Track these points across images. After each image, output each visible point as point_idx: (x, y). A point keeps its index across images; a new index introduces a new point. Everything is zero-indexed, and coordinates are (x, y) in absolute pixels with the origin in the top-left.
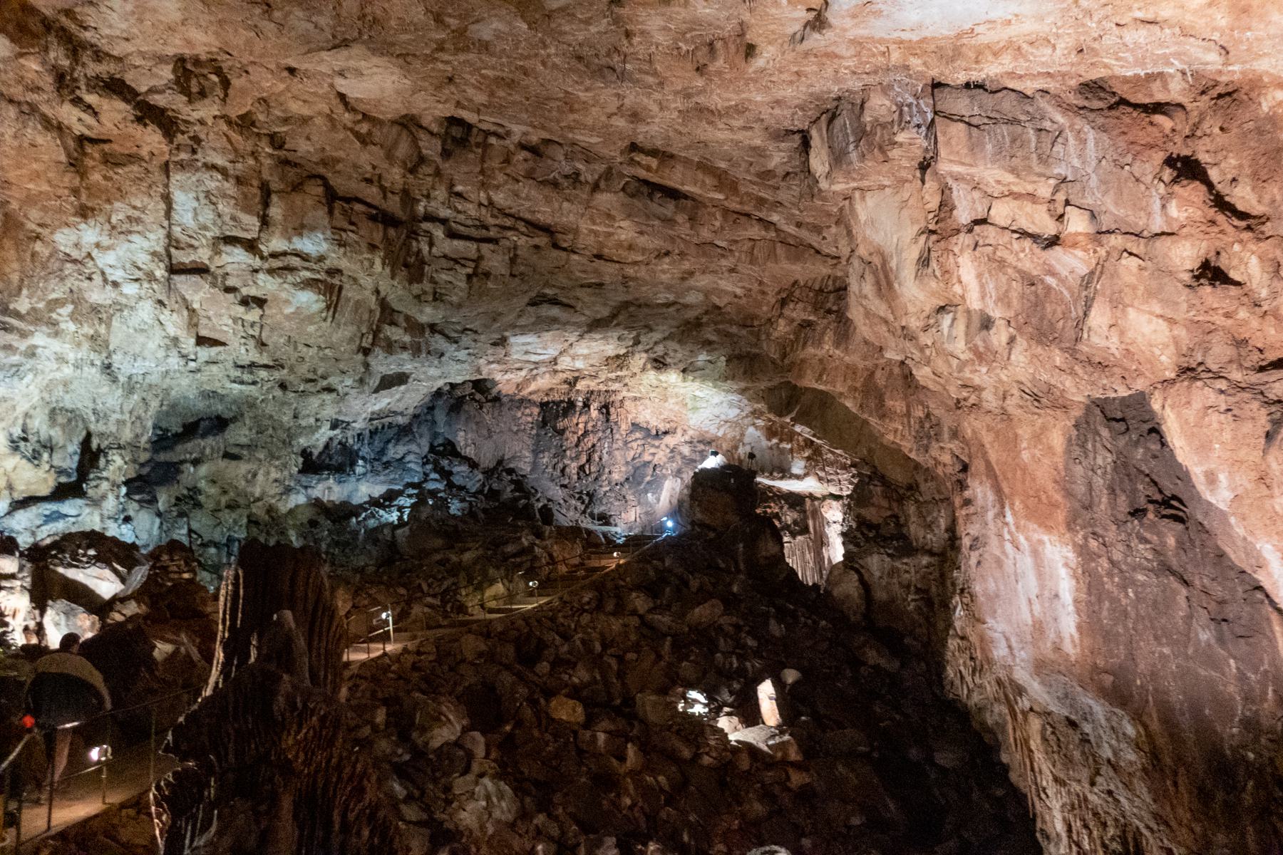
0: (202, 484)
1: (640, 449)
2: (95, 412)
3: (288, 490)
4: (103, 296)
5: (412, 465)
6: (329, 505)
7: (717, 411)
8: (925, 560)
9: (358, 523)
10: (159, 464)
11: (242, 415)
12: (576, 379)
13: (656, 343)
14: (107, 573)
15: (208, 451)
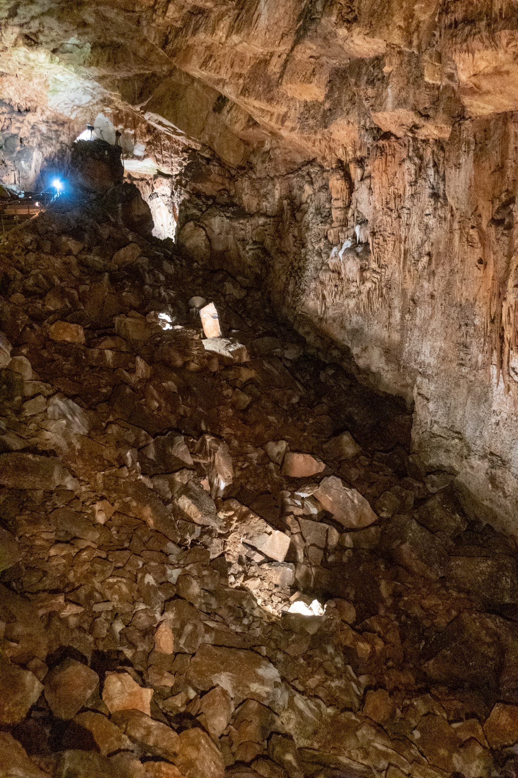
1: (7, 122)
7: (72, 96)
8: (262, 221)
13: (33, 18)
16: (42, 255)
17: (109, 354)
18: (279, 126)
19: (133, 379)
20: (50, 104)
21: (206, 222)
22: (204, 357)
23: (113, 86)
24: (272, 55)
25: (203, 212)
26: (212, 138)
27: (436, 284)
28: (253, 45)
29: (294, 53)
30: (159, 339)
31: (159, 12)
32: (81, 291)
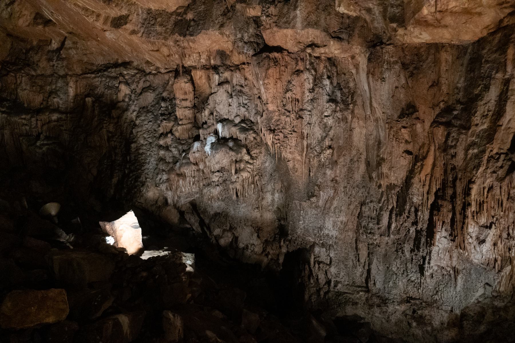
27: (338, 172)
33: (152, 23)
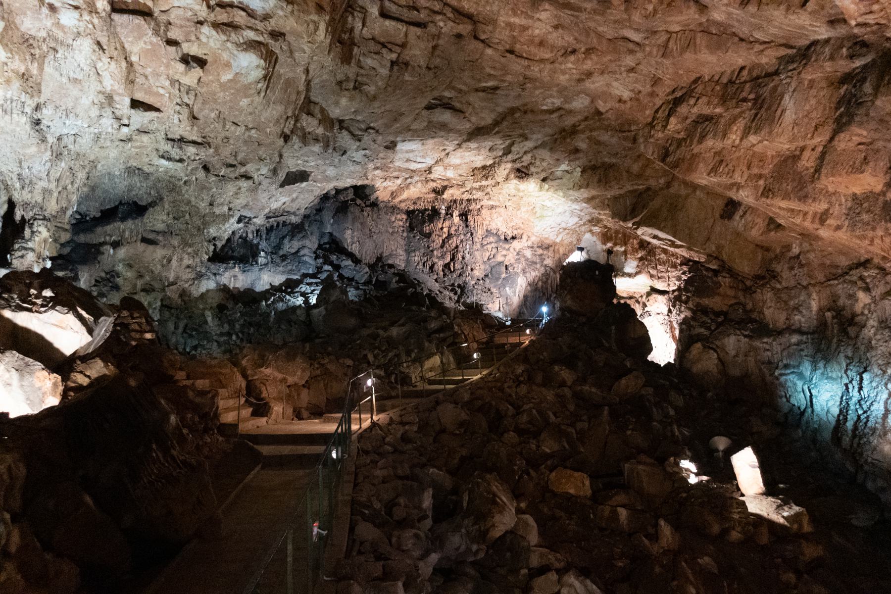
0: (120, 268)
2: (20, 177)
3: (200, 276)
4: (37, 24)
5: (306, 258)
6: (235, 292)
7: (559, 220)
9: (267, 306)
10: (79, 245)
11: (161, 199)
12: (445, 188)
13: (525, 153)
14: (70, 318)
15: (127, 234)
16: (534, 387)
17: (623, 513)
18: (816, 226)
19: (656, 548)
20: (535, 230)
21: (718, 343)
22: (748, 524)
23: (603, 205)
24: (803, 149)
25: (713, 331)
26: (719, 248)
28: (776, 143)
29: (835, 143)
30: (684, 495)
31: (659, 127)
32: (578, 429)
33: (857, 211)
